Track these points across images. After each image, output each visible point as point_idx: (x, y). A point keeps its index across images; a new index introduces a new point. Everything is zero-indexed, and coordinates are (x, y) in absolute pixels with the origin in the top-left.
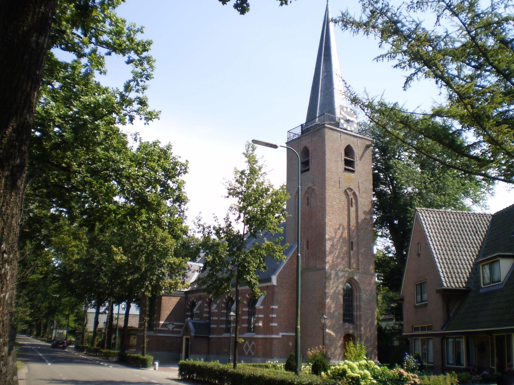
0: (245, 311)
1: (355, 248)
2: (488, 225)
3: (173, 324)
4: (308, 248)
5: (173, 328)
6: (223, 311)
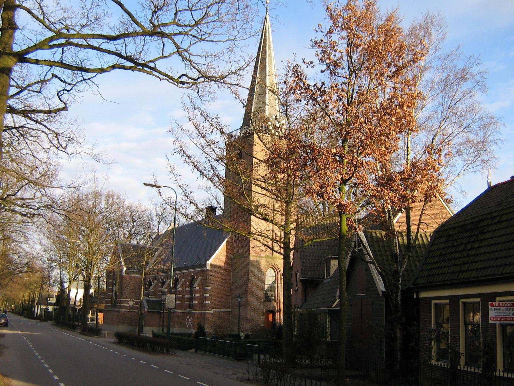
2: (429, 240)
3: (133, 301)
4: (238, 238)
5: (134, 304)
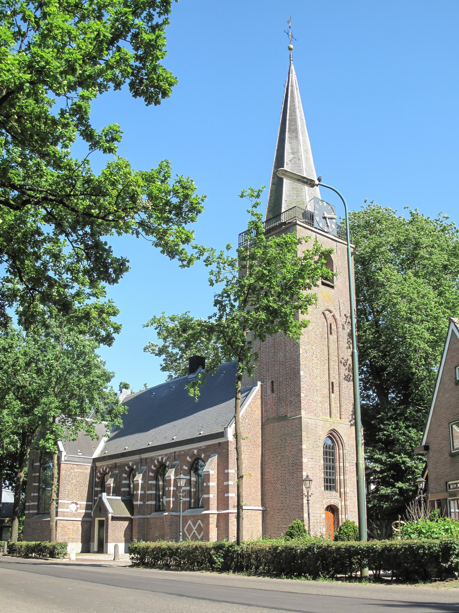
0: (125, 484)
1: (336, 388)
4: (273, 391)
6: (150, 482)
